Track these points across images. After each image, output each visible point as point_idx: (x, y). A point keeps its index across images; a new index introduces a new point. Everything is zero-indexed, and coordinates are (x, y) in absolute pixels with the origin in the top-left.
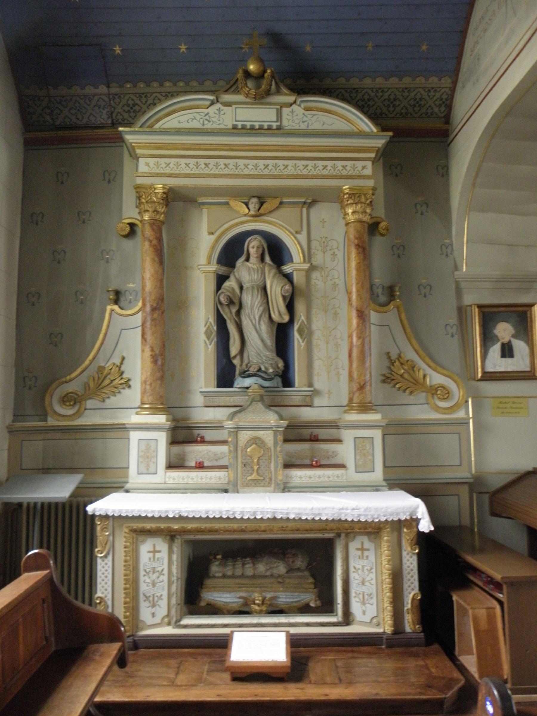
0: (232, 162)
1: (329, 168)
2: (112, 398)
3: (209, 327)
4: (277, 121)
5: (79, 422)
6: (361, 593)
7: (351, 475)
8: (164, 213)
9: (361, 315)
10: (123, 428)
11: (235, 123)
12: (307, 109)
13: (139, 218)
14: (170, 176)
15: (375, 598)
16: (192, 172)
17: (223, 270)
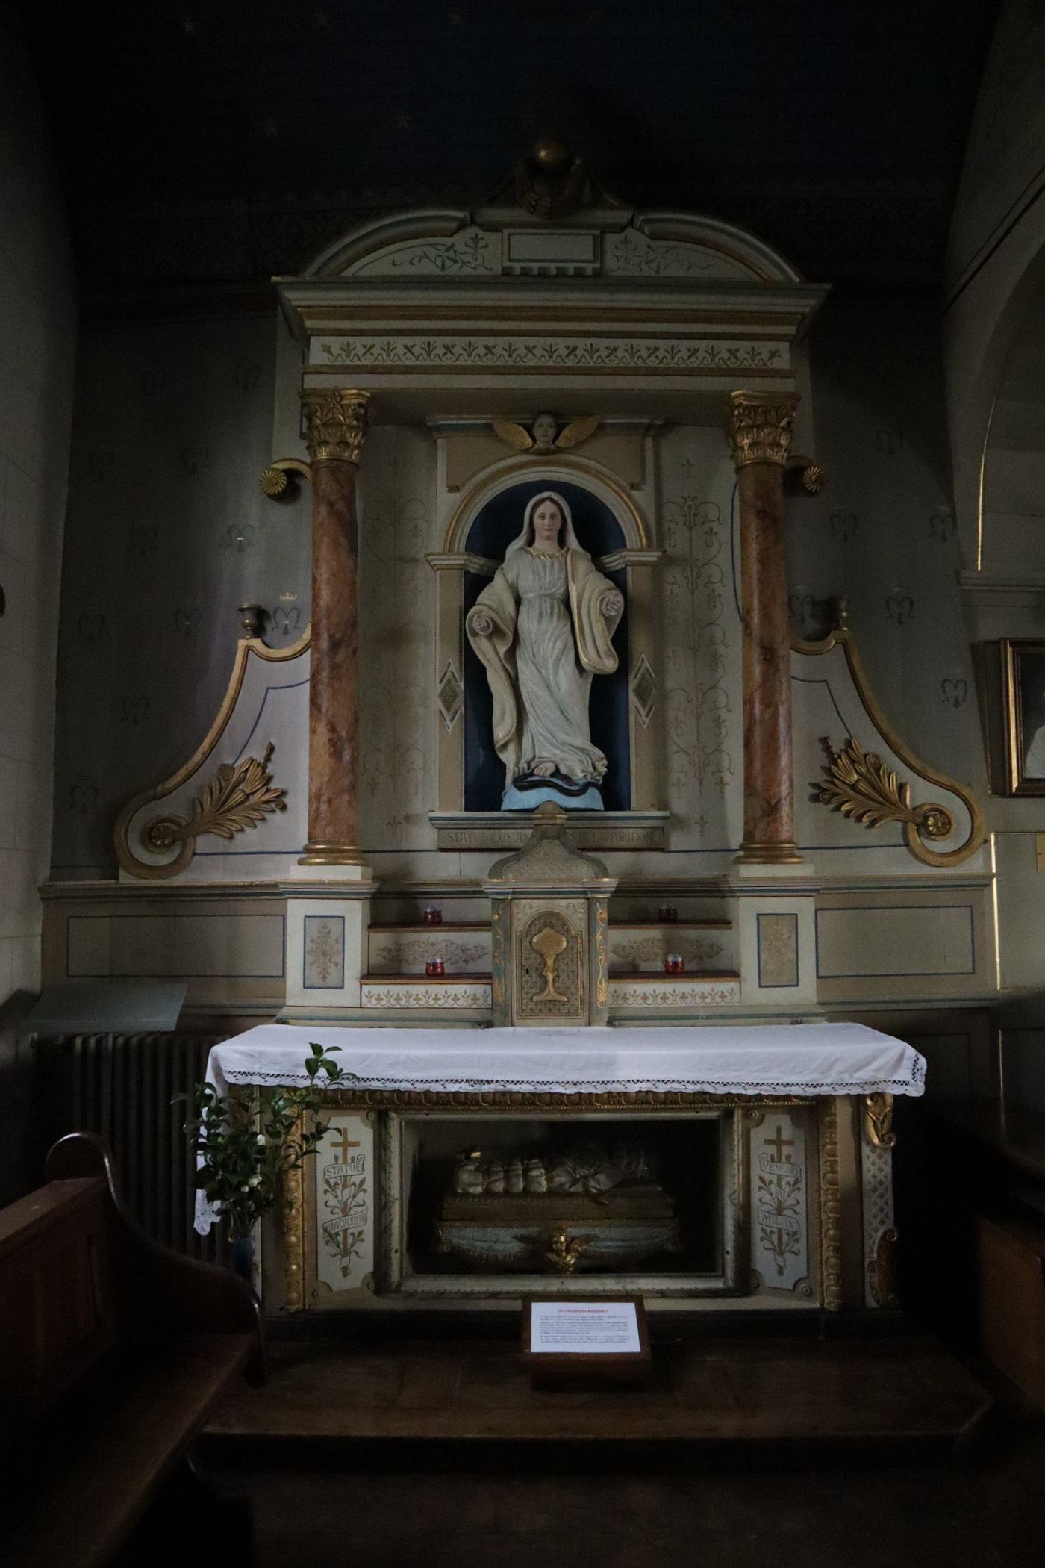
0: (501, 342)
1: (701, 354)
2: (248, 830)
3: (449, 681)
4: (594, 261)
5: (180, 880)
7: (749, 991)
8: (358, 447)
9: (769, 656)
10: (276, 894)
11: (507, 264)
12: (654, 237)
13: (308, 460)
14: (373, 370)
15: (804, 1240)
16: (418, 363)
17: (477, 564)
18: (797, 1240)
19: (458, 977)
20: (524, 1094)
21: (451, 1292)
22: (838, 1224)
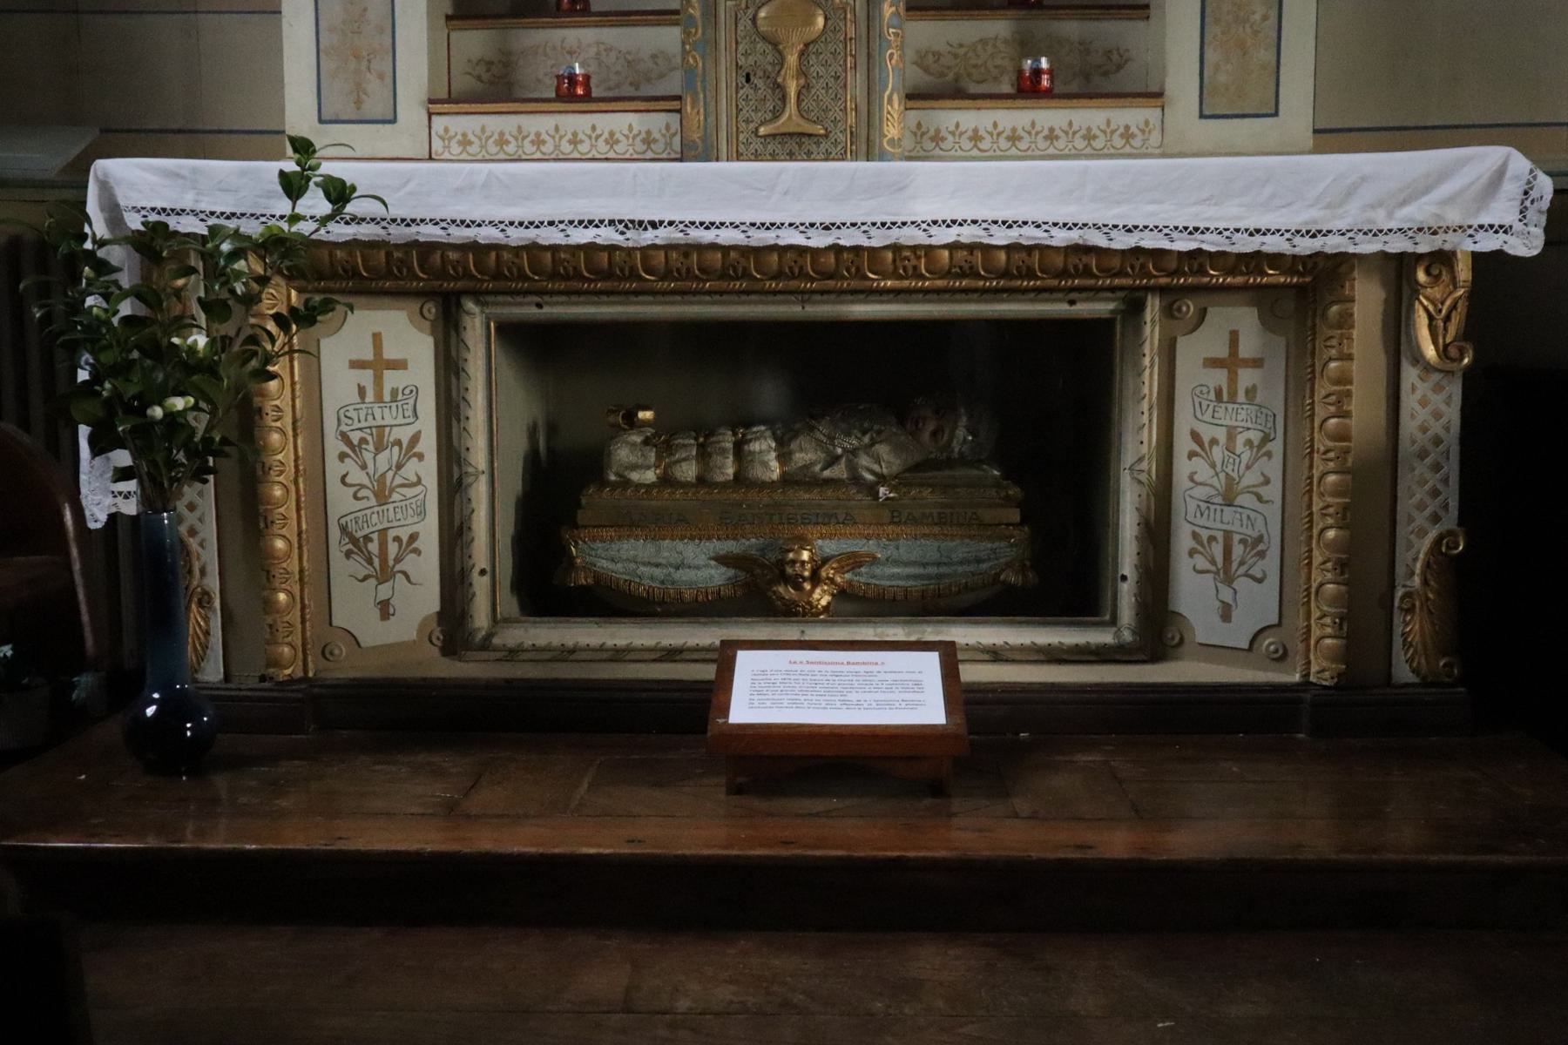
6: (1220, 536)
18: (1262, 555)
19: (615, 101)
20: (726, 250)
21: (588, 648)
22: (1346, 517)
